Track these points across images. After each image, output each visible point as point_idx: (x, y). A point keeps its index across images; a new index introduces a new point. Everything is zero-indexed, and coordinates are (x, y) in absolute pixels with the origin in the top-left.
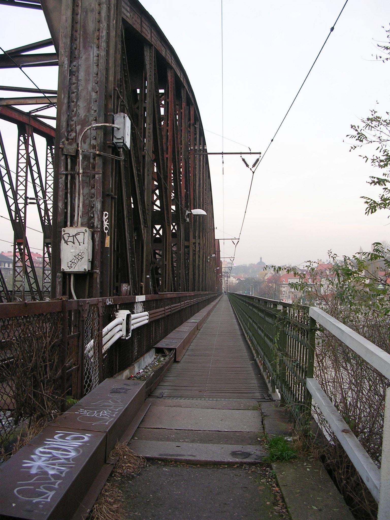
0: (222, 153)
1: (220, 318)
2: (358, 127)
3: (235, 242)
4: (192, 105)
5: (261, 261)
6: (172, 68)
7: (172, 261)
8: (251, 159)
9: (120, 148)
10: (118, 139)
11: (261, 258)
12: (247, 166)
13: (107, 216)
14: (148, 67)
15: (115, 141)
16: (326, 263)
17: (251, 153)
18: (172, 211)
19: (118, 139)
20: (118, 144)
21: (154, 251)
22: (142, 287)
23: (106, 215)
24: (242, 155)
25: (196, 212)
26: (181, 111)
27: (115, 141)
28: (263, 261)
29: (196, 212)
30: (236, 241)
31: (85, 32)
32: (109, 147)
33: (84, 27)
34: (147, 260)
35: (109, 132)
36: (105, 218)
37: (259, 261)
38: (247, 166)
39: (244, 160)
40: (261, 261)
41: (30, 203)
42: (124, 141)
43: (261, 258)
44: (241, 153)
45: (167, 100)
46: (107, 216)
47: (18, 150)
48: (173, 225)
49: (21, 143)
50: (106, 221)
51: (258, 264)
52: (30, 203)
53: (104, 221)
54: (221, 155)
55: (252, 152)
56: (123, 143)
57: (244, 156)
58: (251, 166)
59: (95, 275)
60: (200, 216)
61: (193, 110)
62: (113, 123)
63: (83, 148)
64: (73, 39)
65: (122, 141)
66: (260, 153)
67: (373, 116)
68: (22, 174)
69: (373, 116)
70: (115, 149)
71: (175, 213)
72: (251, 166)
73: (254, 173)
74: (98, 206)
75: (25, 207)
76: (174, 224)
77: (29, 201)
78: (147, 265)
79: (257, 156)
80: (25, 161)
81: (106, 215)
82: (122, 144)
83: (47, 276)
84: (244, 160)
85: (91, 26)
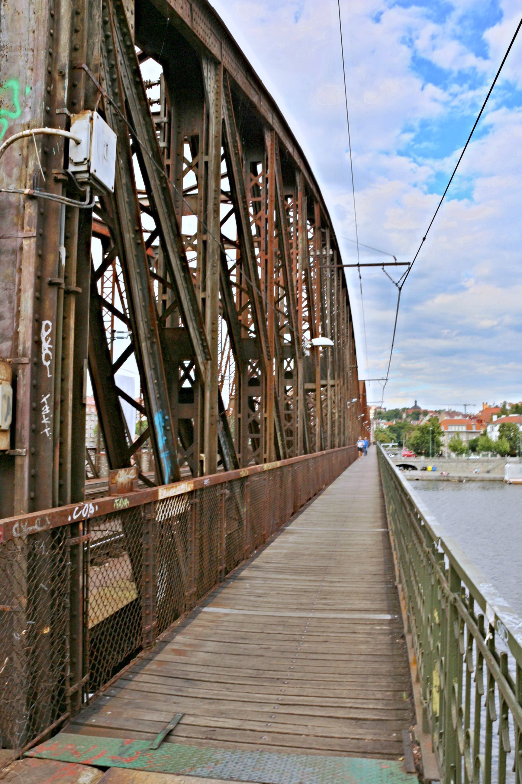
4: (317, 202)
5: (416, 405)
6: (300, 171)
9: (83, 184)
10: (77, 164)
13: (49, 331)
14: (211, 96)
15: (72, 168)
16: (492, 407)
17: (396, 264)
18: (285, 341)
19: (77, 164)
20: (78, 176)
21: (250, 398)
22: (202, 462)
23: (47, 327)
26: (297, 203)
27: (72, 168)
32: (57, 180)
34: (211, 416)
35: (55, 151)
36: (44, 334)
37: (413, 405)
40: (416, 405)
41: (118, 338)
42: (89, 167)
45: (266, 176)
46: (49, 331)
50: (47, 340)
51: (413, 408)
52: (118, 338)
53: (43, 339)
54: (357, 268)
55: (398, 261)
56: (88, 171)
59: (18, 461)
61: (318, 209)
62: (68, 129)
65: (84, 168)
70: (71, 187)
71: (289, 344)
73: (400, 289)
77: (116, 335)
78: (211, 424)
81: (47, 327)
82: (87, 175)
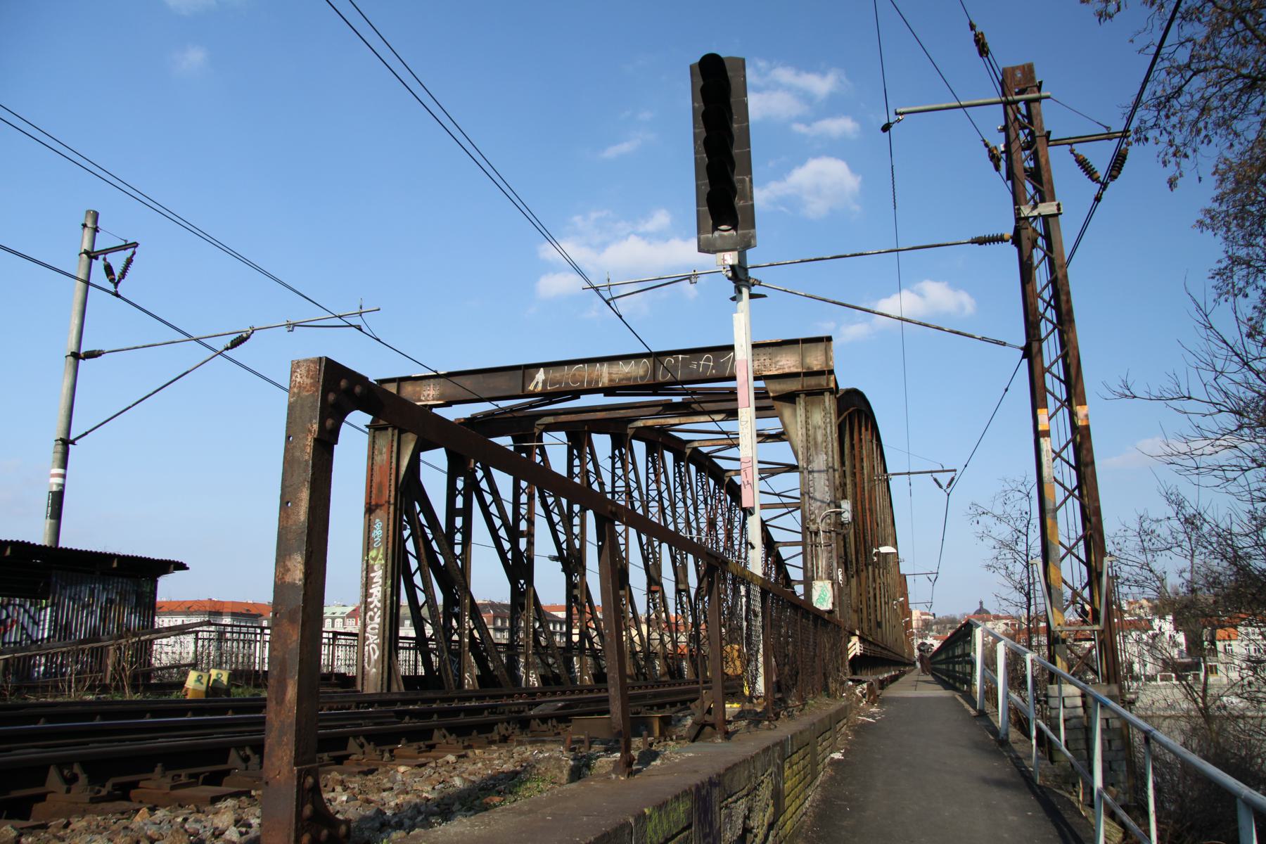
0: (909, 473)
2: (1220, 261)
3: (933, 577)
8: (944, 479)
11: (981, 603)
12: (940, 486)
25: (883, 550)
28: (985, 607)
29: (883, 550)
30: (933, 577)
31: (816, 443)
33: (815, 439)
37: (978, 607)
38: (940, 486)
39: (936, 480)
43: (981, 603)
63: (822, 527)
64: (808, 449)
68: (524, 498)
74: (835, 565)
79: (952, 474)
83: (1069, 551)
84: (936, 480)
85: (820, 439)
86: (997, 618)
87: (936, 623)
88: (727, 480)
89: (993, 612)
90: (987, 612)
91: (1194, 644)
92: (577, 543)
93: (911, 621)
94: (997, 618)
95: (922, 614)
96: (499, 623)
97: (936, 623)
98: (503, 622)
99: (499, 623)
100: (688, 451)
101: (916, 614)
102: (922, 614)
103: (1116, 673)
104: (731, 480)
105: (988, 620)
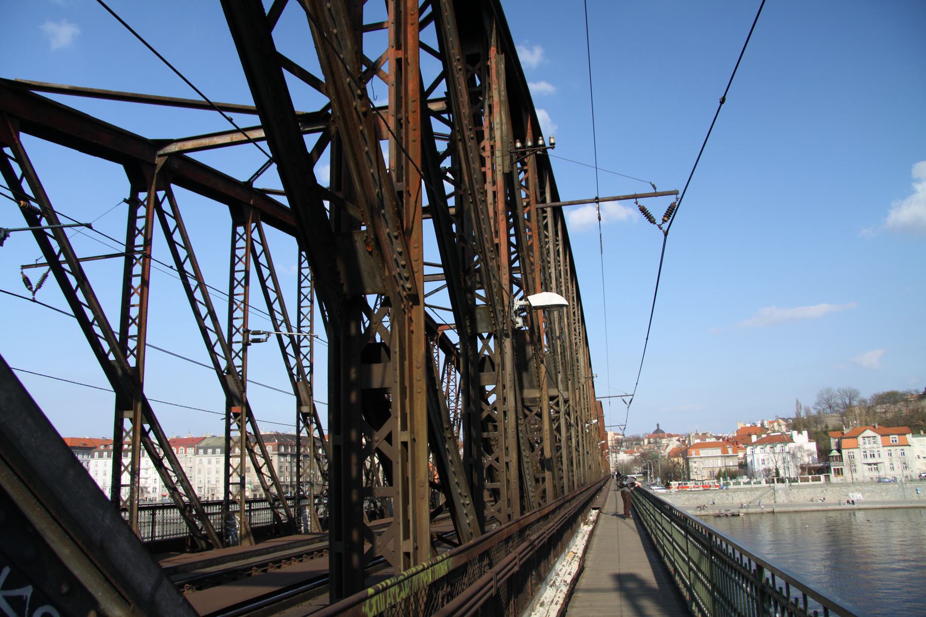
1: (594, 552)
3: (628, 399)
7: (426, 114)
12: (651, 220)
24: (638, 200)
25: (539, 299)
29: (539, 299)
30: (629, 400)
38: (651, 220)
44: (635, 197)
47: (300, 288)
48: (482, 338)
49: (303, 259)
57: (641, 201)
58: (659, 221)
60: (547, 309)
66: (676, 193)
67: (892, 473)
69: (892, 473)
72: (659, 221)
73: (666, 234)
75: (244, 350)
76: (485, 335)
79: (672, 199)
80: (302, 350)
84: (643, 210)
86: (670, 436)
87: (626, 441)
88: (440, 333)
89: (666, 432)
90: (663, 432)
91: (824, 453)
92: (132, 361)
93: (607, 443)
94: (670, 436)
95: (615, 434)
96: (283, 449)
97: (626, 441)
98: (286, 448)
99: (283, 449)
100: (160, 162)
101: (610, 436)
102: (615, 434)
103: (244, 332)
104: (443, 333)
105: (663, 438)
